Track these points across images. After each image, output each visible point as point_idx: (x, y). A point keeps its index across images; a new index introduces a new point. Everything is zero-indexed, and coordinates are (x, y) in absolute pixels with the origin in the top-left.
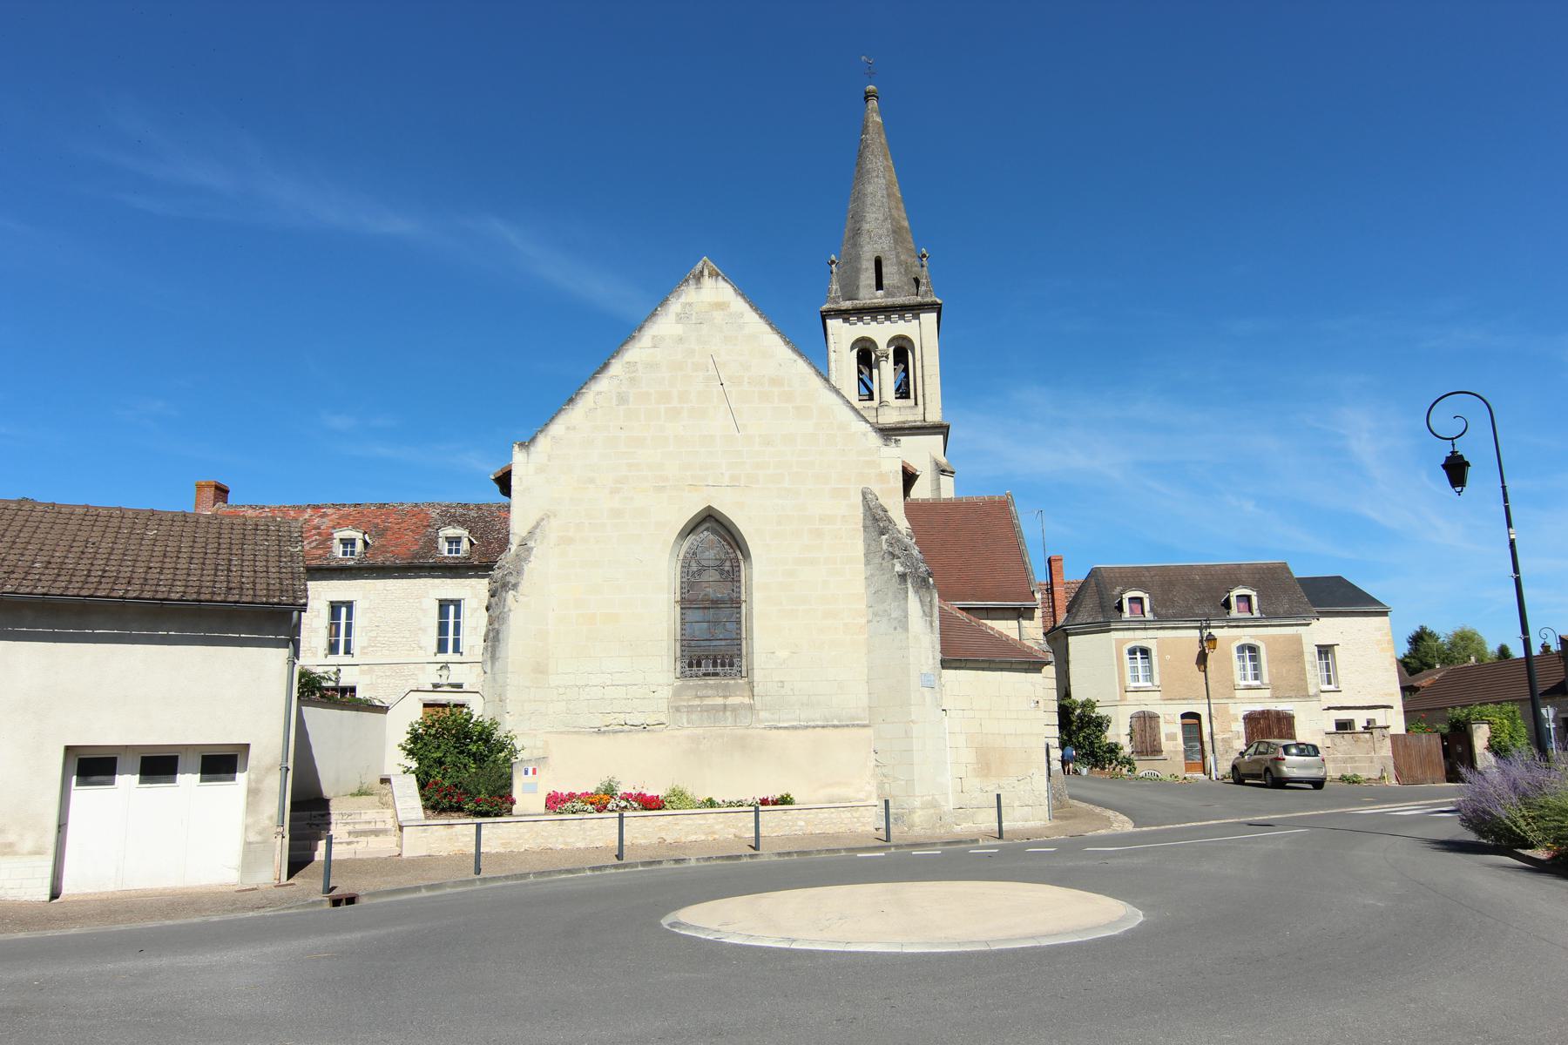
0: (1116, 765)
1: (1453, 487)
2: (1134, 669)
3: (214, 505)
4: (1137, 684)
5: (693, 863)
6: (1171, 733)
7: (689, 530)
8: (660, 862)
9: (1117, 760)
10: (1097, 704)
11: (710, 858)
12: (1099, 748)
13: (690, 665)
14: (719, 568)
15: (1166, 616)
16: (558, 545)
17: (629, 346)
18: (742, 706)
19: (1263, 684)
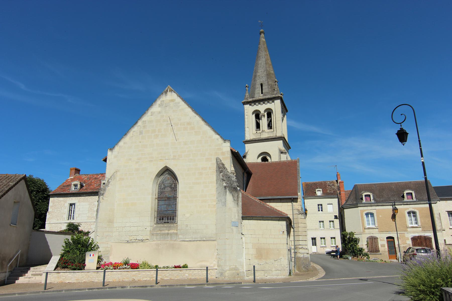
1: (402, 142)
2: (368, 221)
3: (75, 175)
5: (128, 288)
6: (383, 245)
7: (161, 174)
8: (115, 287)
9: (362, 254)
10: (355, 234)
11: (135, 286)
12: (356, 249)
13: (160, 220)
14: (171, 187)
15: (379, 201)
16: (119, 181)
17: (144, 116)
18: (174, 233)
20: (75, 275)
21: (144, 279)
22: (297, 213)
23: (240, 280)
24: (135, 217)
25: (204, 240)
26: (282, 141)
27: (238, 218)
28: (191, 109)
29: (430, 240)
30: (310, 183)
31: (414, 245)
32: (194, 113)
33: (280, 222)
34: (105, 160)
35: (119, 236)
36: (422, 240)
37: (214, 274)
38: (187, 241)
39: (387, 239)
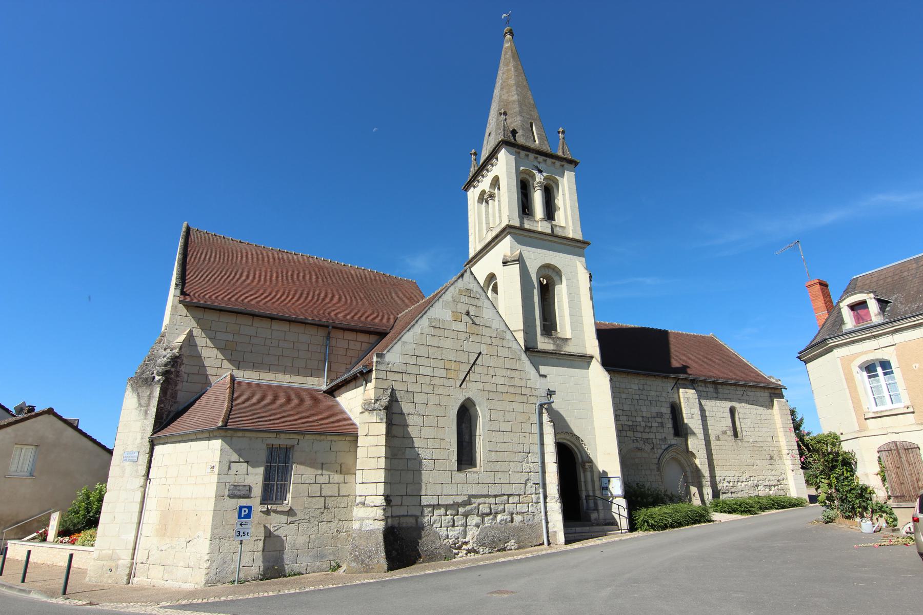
4: (880, 408)
27: (141, 443)
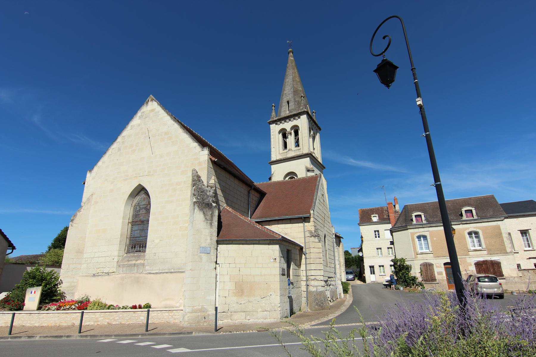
0: (416, 286)
2: (421, 244)
5: (37, 338)
7: (136, 194)
8: (20, 337)
9: (416, 284)
10: (406, 260)
12: (408, 278)
13: (132, 248)
19: (483, 248)
20: (4, 317)
21: (86, 324)
22: (309, 235)
23: (207, 325)
24: (104, 245)
25: (171, 272)
26: (308, 158)
27: (211, 242)
28: (170, 117)
29: (498, 265)
30: (366, 210)
31: (479, 272)
32: (173, 121)
33: (271, 246)
34: (84, 183)
35: (87, 268)
36: (488, 265)
37: (178, 317)
38: (153, 273)
39: (444, 265)
